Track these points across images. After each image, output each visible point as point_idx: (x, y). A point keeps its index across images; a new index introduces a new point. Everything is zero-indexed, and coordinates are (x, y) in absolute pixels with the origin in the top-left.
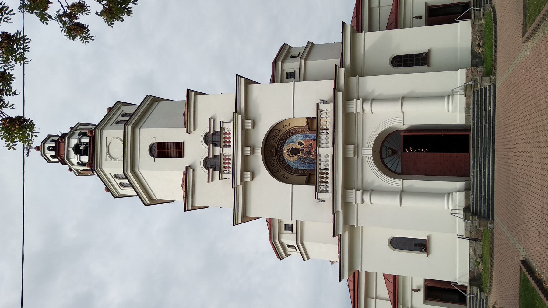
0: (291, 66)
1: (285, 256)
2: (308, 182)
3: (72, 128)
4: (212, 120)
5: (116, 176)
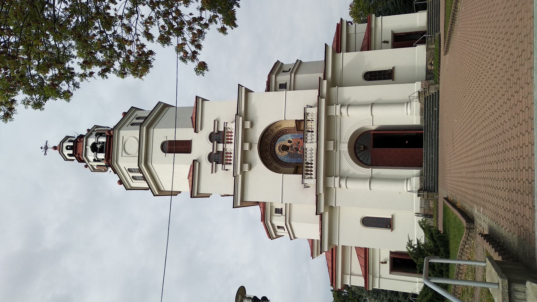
0: (283, 78)
1: (275, 237)
2: (296, 172)
3: (88, 130)
4: (216, 122)
5: (130, 170)
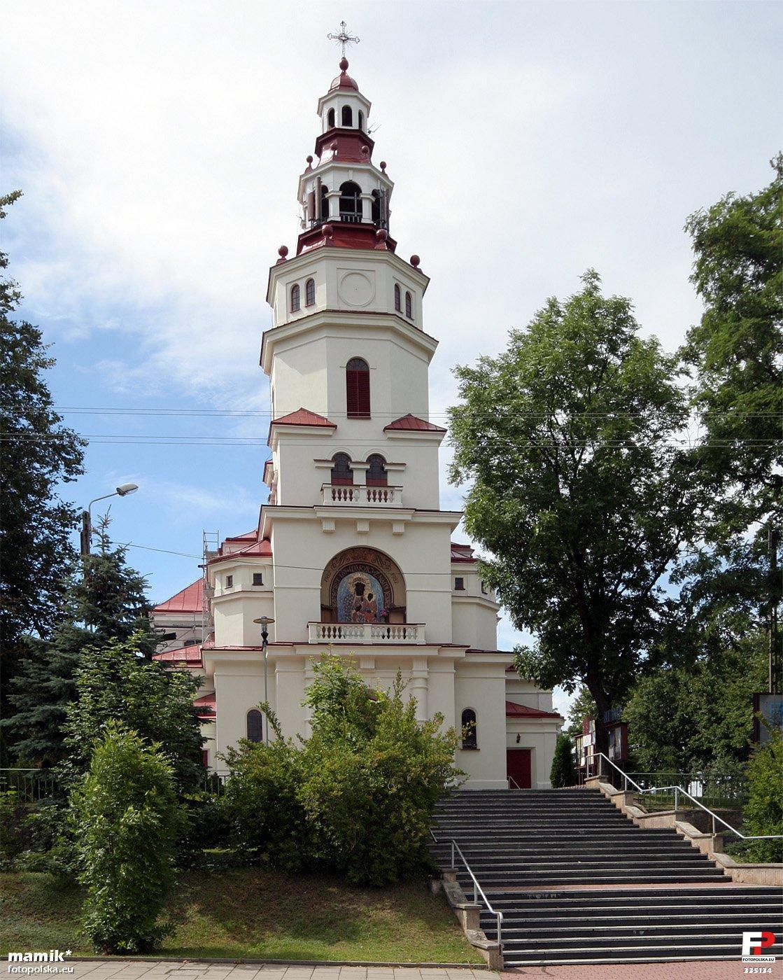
2: (323, 608)
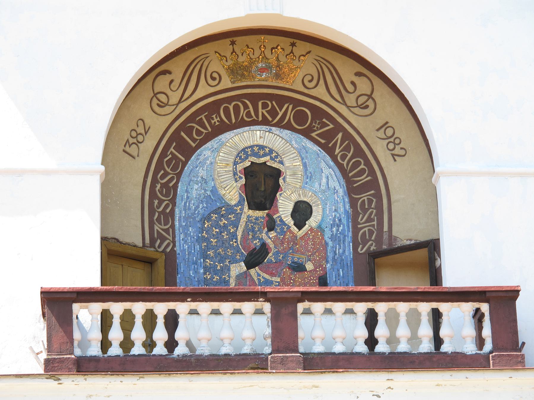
2: (113, 252)
